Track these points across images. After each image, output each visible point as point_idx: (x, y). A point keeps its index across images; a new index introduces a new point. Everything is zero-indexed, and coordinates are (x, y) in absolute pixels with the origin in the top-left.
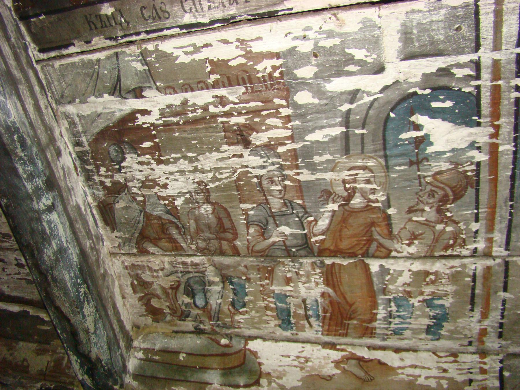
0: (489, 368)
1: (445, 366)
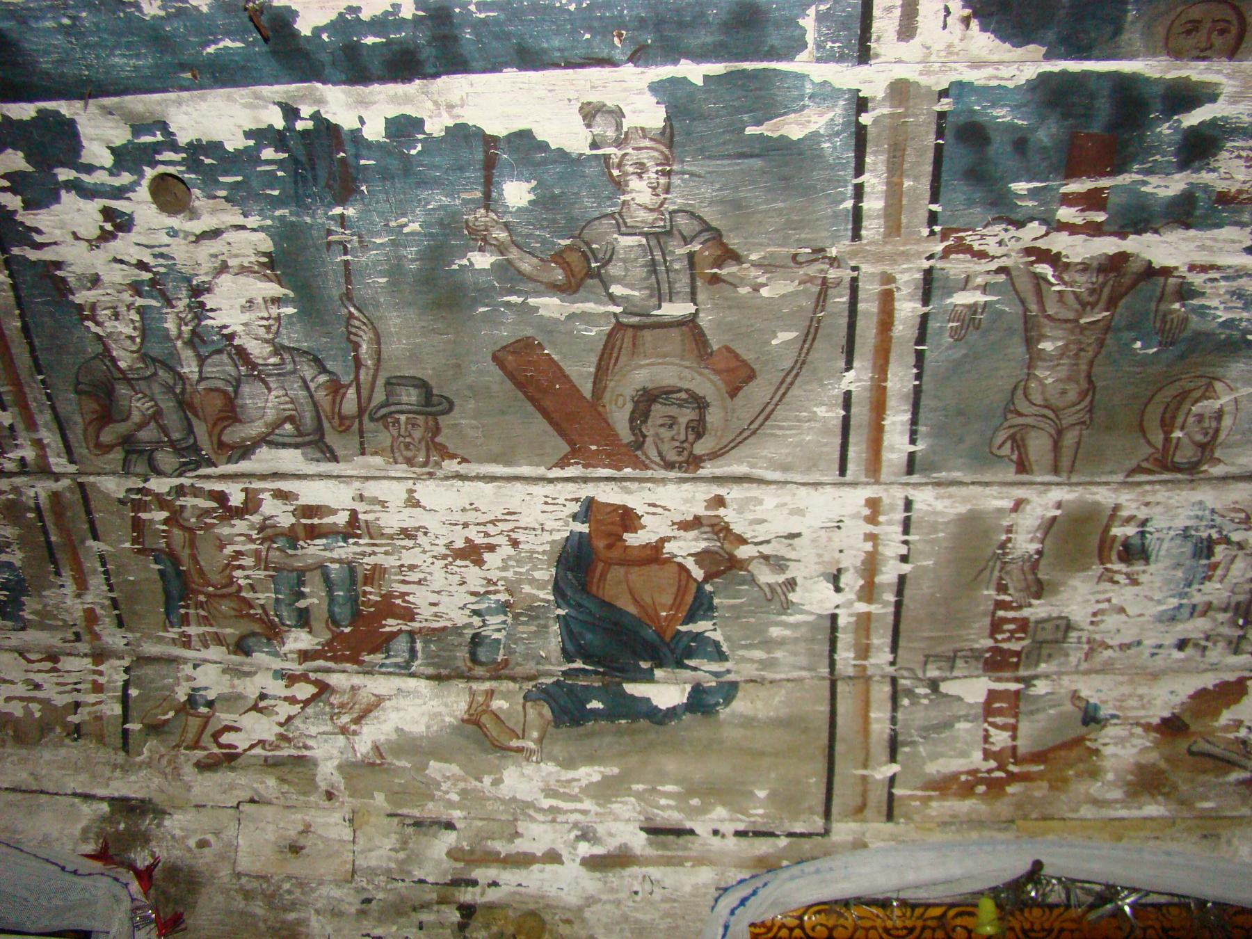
0: (108, 682)
1: (38, 678)
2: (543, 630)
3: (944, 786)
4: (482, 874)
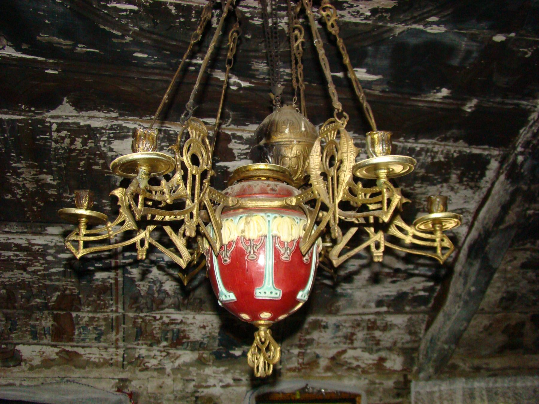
1: (102, 353)
2: (215, 342)
3: (291, 370)
4: (200, 390)
